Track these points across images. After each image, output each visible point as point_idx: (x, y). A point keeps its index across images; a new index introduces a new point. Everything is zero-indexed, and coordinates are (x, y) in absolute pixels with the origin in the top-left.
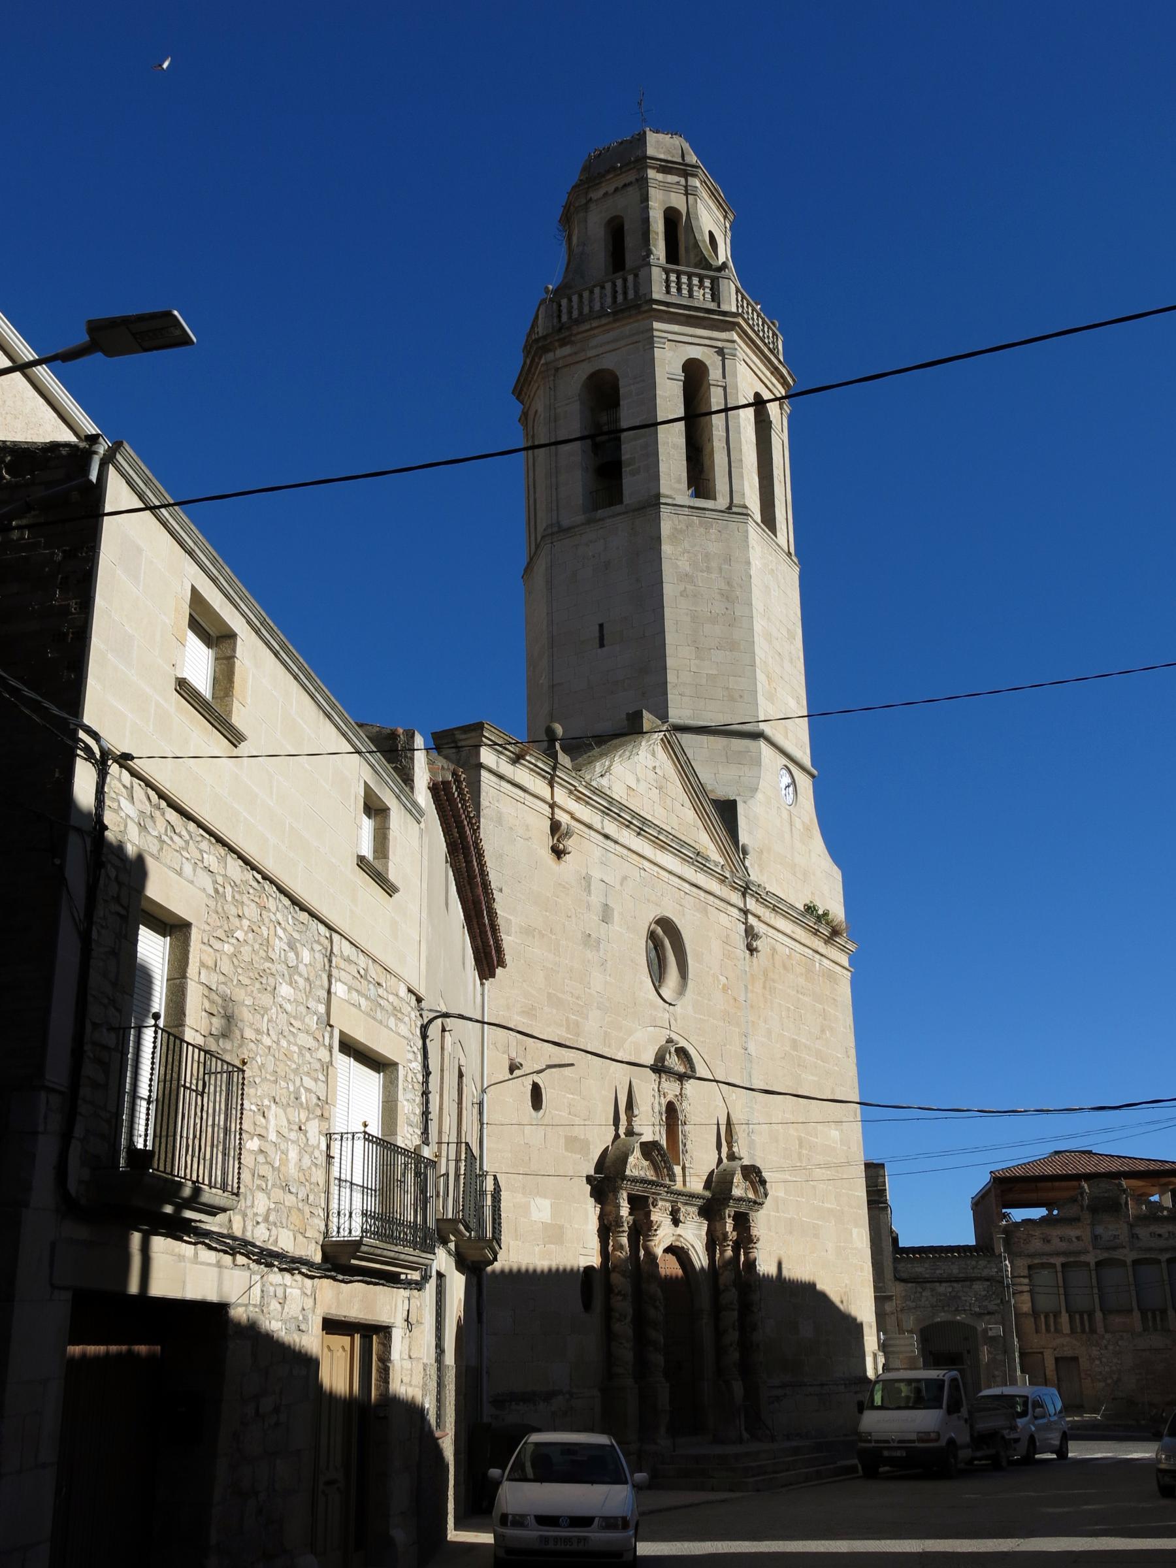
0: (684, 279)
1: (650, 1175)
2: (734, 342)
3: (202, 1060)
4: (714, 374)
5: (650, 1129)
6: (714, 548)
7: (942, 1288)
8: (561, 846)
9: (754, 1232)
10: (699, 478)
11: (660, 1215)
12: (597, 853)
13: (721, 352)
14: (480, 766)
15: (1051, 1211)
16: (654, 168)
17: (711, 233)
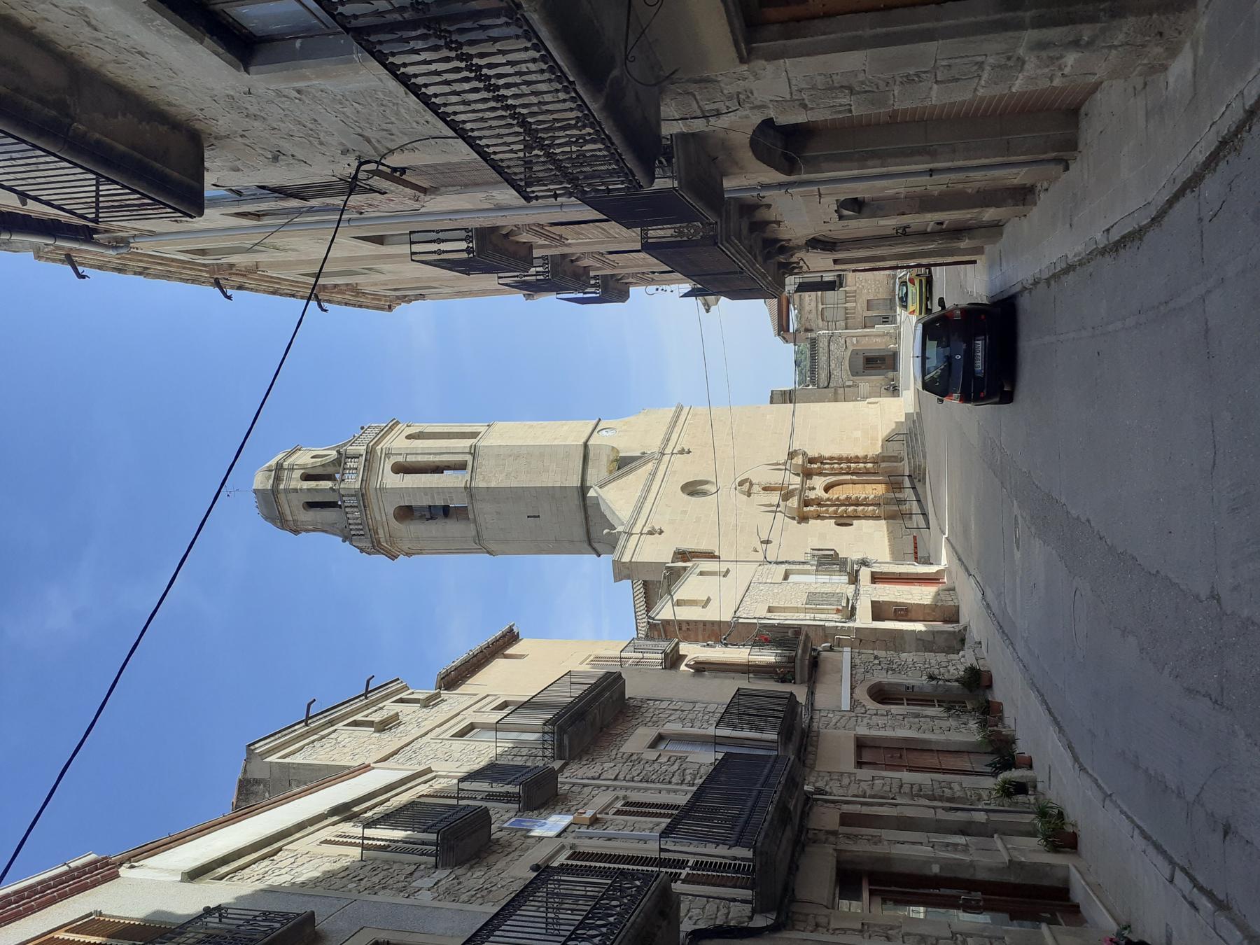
1: (796, 498)
3: (562, 933)
4: (400, 459)
5: (775, 498)
7: (833, 366)
11: (812, 495)
13: (388, 455)
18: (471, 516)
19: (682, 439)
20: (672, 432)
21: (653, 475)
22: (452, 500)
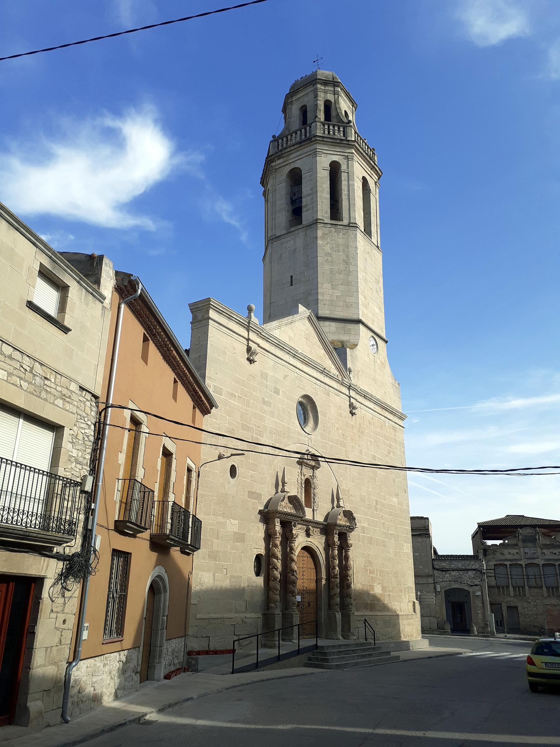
0: (331, 128)
4: (344, 167)
5: (294, 489)
6: (341, 241)
7: (454, 573)
8: (251, 358)
9: (350, 542)
10: (335, 211)
11: (298, 531)
12: (271, 363)
13: (347, 158)
14: (209, 318)
15: (504, 541)
16: (319, 83)
17: (345, 111)
18: (293, 229)
19: (365, 411)
20: (375, 403)
21: (323, 372)
22: (306, 211)
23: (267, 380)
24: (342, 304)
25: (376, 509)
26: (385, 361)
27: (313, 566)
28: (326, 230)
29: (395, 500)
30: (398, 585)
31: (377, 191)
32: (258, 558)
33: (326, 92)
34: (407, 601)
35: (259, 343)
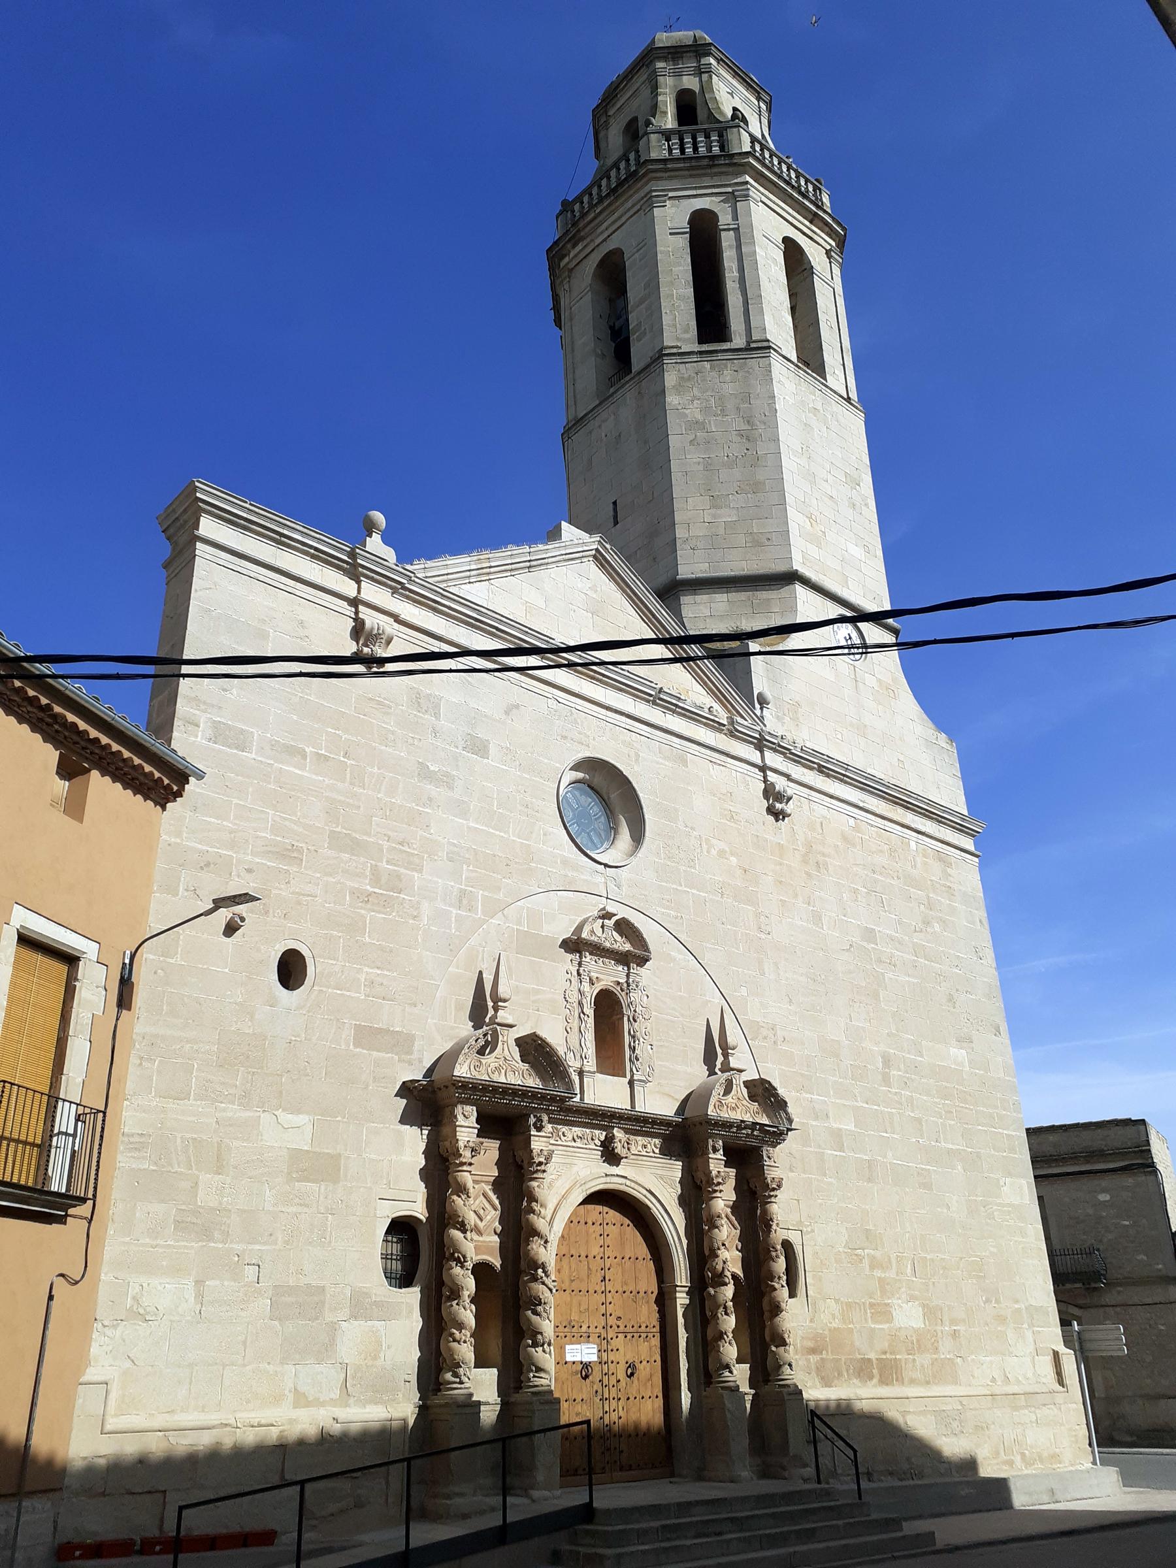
2: (747, 183)
4: (725, 219)
6: (729, 389)
9: (771, 1174)
10: (712, 320)
20: (864, 787)
22: (639, 339)
23: (437, 716)
24: (741, 540)
25: (886, 1080)
26: (894, 680)
27: (643, 1250)
28: (687, 370)
29: (958, 1054)
30: (988, 1301)
31: (837, 271)
32: (401, 1228)
33: (678, 75)
34: (1031, 1348)
35: (789, 772)
